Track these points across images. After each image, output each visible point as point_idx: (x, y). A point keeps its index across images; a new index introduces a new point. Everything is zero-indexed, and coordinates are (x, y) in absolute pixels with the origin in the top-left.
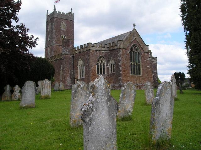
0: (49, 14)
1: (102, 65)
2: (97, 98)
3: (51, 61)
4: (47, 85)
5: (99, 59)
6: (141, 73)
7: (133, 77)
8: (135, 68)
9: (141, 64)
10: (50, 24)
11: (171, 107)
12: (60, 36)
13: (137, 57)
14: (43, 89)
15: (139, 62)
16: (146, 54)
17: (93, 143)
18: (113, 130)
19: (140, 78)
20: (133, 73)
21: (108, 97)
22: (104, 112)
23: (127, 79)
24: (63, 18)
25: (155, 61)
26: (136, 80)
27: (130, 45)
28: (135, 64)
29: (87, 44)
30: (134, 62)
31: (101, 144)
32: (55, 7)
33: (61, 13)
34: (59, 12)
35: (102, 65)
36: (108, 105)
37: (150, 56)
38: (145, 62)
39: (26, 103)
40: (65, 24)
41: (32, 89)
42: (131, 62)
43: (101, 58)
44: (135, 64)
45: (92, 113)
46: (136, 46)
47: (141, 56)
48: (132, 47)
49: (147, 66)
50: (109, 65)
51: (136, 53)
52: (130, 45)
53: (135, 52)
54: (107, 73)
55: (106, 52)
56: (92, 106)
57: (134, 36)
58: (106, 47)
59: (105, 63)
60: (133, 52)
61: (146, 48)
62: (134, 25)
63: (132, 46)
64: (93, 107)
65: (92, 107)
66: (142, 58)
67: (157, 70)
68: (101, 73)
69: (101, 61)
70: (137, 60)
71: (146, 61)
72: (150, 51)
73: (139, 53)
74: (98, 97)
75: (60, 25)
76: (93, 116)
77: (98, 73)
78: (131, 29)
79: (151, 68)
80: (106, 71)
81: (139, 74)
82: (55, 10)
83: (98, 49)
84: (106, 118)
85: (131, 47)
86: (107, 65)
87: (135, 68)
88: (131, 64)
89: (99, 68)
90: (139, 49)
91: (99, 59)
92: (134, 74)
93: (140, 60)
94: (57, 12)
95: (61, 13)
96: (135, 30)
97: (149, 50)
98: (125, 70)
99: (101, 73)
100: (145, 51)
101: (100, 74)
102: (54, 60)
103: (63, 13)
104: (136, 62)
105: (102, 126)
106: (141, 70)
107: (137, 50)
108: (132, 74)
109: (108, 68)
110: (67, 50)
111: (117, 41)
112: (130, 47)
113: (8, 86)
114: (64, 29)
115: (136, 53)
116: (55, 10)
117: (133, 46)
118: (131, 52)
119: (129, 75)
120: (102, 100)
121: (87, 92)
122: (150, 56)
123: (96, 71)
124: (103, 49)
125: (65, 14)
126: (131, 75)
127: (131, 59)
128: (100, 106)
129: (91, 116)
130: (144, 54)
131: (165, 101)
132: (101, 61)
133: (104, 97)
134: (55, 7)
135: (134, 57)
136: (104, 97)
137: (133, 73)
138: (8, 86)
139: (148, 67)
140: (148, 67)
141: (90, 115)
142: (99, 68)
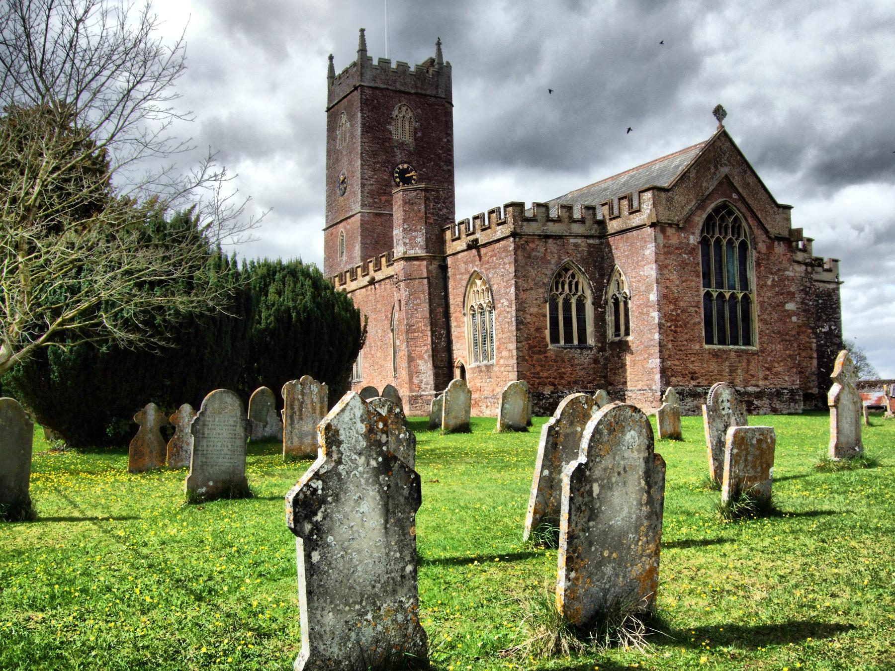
0: (338, 72)
1: (573, 301)
2: (339, 462)
3: (348, 289)
4: (312, 402)
5: (559, 275)
6: (756, 338)
7: (716, 355)
8: (727, 314)
9: (754, 297)
10: (344, 118)
11: (648, 492)
12: (392, 174)
13: (737, 263)
14: (296, 417)
15: (745, 284)
16: (780, 249)
17: (328, 601)
18: (401, 565)
19: (749, 362)
20: (716, 340)
21: (380, 459)
22: (365, 507)
23: (686, 367)
24: (402, 88)
25: (827, 276)
26: (733, 371)
27: (701, 206)
28: (727, 296)
29: (348, 279)
30: (720, 285)
31: (357, 607)
32: (362, 37)
33: (394, 66)
34: (384, 62)
35: (573, 301)
36: (380, 485)
37: (800, 256)
38: (773, 286)
39: (209, 480)
40: (410, 114)
41: (232, 423)
42: (707, 284)
43: (566, 270)
44: (727, 296)
45: (323, 509)
46: (730, 213)
47: (752, 256)
48: (710, 218)
49: (783, 304)
50: (606, 302)
51: (730, 242)
52: (701, 206)
53: (725, 242)
54: (598, 341)
55: (591, 241)
56: (320, 487)
57: (717, 163)
58: (589, 222)
59: (588, 293)
60: (718, 242)
61: (778, 218)
62: (719, 112)
63: (709, 210)
64: (323, 489)
65: (320, 492)
66: (758, 265)
67: (837, 322)
68: (569, 338)
69: (567, 287)
70: (737, 278)
71: (782, 280)
72: (799, 231)
73: (743, 246)
74: (340, 458)
75: (389, 119)
76: (324, 518)
77: (555, 339)
78: (706, 133)
79: (804, 311)
80: (590, 328)
81: (748, 342)
82: (363, 50)
83: (553, 229)
84: (693, 551)
85: (705, 216)
86: (597, 303)
87: (727, 314)
88: (708, 295)
89: (561, 317)
90: (744, 224)
91: (559, 275)
92: (722, 342)
93: (752, 275)
94: (375, 62)
95: (394, 66)
96: (723, 136)
97: (794, 226)
98: (676, 326)
99: (569, 338)
100: (773, 231)
101: (562, 343)
102: (362, 284)
103: (403, 66)
104: (732, 287)
105: (359, 552)
106: (756, 326)
107: (737, 229)
108: (709, 341)
109: (600, 319)
110: (416, 237)
111: (640, 192)
112: (700, 219)
113: (151, 407)
114: (408, 138)
115: (730, 242)
116: (363, 50)
117: (717, 210)
118: (704, 242)
119: (697, 347)
120: (356, 468)
121: (402, 436)
122: (800, 256)
123: (547, 332)
124: (577, 228)
125: (412, 69)
126: (707, 347)
127: (706, 276)
128: (352, 487)
129: (319, 517)
130: (770, 248)
131: (619, 474)
132: (567, 287)
133: (363, 458)
134: (362, 37)
135: (719, 263)
136: (363, 458)
137: (716, 340)
138: (151, 407)
139: (790, 306)
140: (790, 306)
141: (316, 515)
142: (561, 317)
